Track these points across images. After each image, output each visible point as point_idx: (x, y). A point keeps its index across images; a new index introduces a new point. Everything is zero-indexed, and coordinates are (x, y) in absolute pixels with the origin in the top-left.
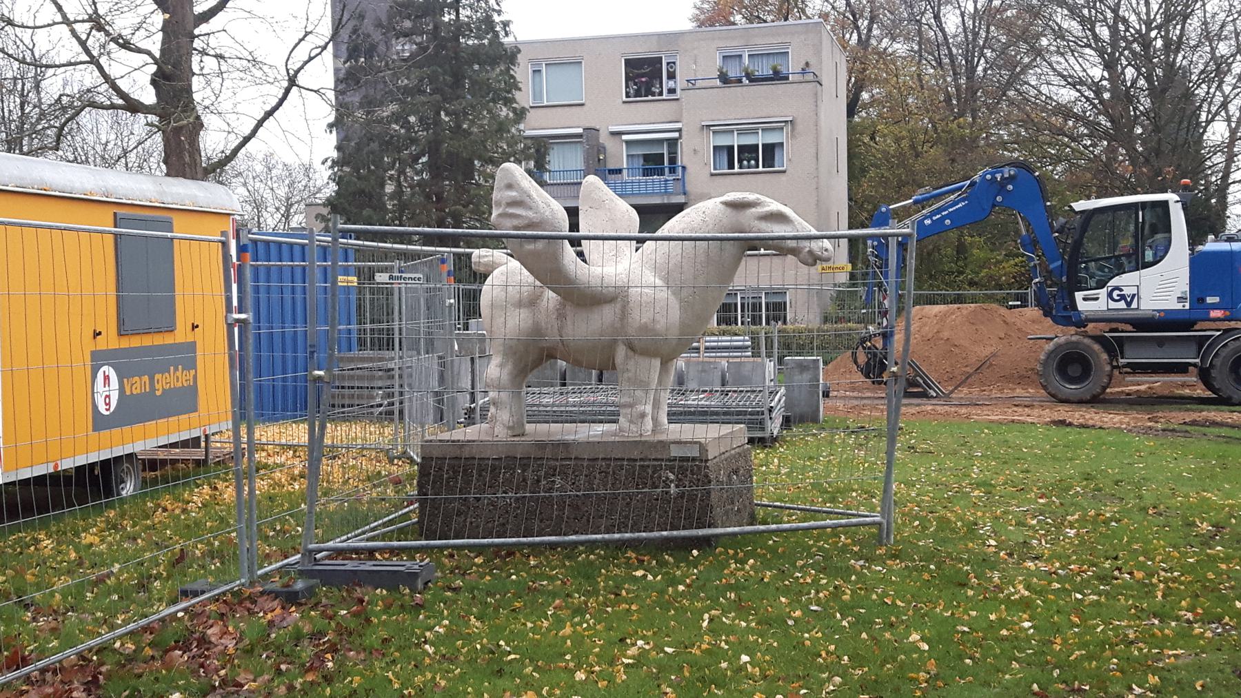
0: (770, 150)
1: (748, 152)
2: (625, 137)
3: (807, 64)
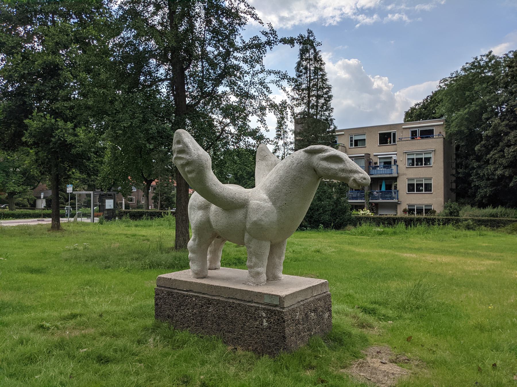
0: (428, 160)
1: (419, 160)
2: (378, 156)
3: (440, 133)
